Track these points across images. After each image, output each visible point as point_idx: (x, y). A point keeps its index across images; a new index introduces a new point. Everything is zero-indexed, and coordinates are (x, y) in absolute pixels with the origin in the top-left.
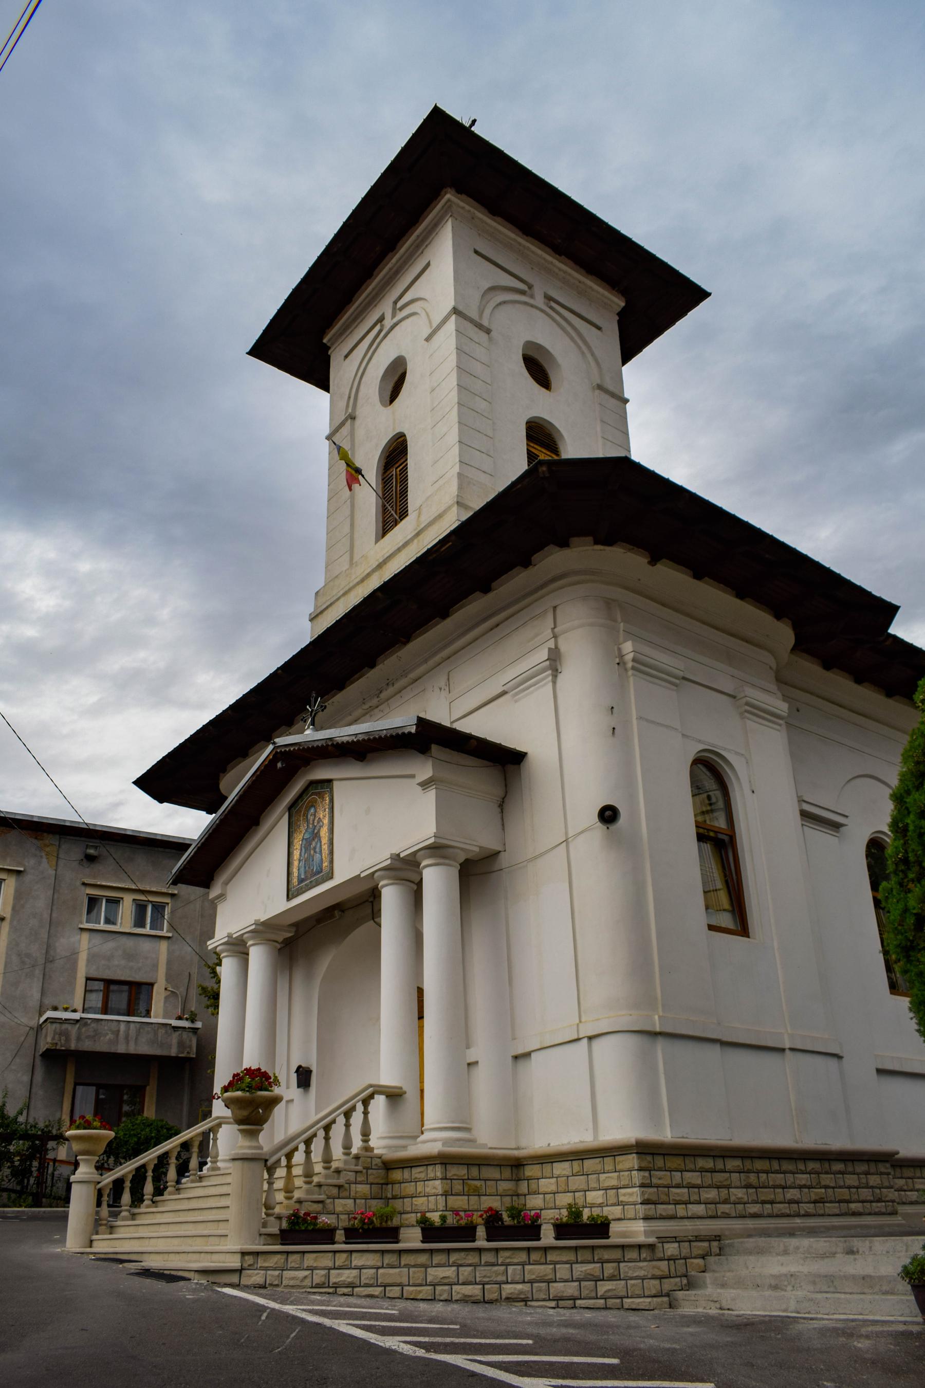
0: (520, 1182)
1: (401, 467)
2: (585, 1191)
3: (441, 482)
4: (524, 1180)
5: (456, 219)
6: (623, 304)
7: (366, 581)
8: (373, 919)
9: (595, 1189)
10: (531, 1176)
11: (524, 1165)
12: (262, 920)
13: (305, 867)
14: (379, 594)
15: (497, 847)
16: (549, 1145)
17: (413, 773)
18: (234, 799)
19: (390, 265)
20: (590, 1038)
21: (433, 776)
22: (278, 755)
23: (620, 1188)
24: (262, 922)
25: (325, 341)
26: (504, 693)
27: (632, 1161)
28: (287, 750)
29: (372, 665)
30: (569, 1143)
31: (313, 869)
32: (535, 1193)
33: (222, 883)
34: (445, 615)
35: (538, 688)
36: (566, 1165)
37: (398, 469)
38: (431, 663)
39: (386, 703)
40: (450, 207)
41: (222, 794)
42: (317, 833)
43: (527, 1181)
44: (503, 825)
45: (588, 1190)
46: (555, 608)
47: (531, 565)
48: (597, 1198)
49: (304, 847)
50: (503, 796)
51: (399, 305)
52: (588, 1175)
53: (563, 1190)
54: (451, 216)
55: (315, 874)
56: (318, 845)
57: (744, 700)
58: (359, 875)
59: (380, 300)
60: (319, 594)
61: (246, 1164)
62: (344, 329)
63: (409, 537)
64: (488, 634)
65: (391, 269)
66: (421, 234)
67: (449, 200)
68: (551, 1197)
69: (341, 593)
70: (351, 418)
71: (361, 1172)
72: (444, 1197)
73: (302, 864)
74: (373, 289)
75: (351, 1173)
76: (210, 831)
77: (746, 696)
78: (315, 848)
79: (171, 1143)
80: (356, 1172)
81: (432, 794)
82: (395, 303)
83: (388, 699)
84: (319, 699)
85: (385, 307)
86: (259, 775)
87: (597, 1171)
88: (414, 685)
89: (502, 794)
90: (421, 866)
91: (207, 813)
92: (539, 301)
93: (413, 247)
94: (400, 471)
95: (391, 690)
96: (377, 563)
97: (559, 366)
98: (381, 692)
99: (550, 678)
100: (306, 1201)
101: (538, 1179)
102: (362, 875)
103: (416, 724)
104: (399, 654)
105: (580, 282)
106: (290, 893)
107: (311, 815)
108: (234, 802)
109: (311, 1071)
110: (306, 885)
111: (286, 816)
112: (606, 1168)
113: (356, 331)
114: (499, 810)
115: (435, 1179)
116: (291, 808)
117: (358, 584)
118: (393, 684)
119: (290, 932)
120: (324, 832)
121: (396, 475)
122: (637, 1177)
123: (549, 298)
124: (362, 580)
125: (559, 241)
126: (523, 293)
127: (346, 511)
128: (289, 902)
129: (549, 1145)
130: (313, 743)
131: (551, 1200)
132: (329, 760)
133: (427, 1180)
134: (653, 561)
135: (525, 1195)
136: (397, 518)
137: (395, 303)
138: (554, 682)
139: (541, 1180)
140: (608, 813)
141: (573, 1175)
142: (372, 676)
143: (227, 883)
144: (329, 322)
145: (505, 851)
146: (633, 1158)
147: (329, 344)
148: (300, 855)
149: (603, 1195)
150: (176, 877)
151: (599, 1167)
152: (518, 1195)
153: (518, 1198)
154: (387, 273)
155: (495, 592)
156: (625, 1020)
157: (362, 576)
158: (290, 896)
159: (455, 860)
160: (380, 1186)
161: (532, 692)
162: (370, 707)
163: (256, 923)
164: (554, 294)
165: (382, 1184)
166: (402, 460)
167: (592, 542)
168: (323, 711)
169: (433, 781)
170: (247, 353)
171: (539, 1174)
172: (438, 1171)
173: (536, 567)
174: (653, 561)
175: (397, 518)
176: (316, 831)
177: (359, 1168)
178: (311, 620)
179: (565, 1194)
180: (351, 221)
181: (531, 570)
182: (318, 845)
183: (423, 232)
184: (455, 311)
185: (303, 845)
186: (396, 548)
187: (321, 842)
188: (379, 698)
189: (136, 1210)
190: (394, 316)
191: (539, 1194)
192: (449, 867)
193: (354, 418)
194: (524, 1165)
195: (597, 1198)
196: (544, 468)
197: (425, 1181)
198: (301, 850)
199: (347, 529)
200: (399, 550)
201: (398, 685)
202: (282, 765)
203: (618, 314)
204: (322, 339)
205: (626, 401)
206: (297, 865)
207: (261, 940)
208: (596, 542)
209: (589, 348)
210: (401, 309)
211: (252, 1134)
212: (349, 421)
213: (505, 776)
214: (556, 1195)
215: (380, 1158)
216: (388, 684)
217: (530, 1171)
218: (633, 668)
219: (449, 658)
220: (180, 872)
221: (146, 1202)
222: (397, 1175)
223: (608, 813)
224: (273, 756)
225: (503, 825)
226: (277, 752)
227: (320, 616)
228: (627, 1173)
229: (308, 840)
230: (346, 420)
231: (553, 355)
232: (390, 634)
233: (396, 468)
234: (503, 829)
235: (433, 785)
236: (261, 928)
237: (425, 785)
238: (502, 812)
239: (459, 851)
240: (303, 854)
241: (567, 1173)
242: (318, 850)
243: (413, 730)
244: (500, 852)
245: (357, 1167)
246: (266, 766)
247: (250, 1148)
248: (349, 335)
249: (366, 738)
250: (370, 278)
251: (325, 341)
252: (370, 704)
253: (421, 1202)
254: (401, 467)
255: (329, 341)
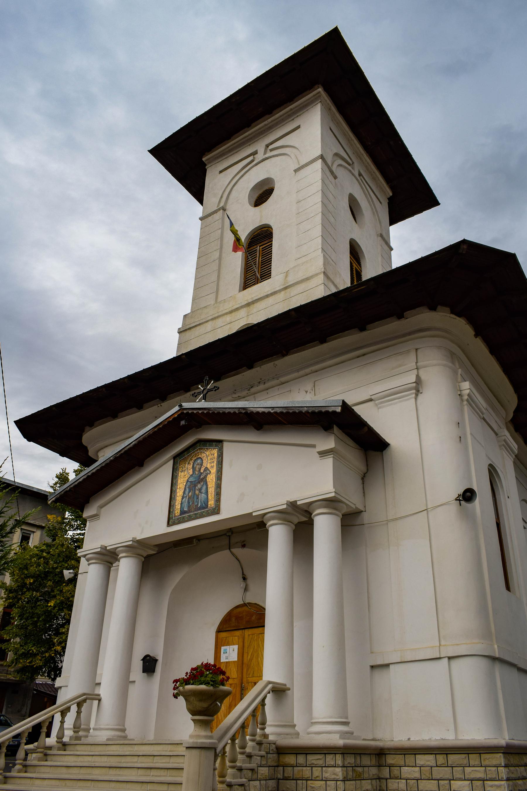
0: (382, 768)
1: (264, 246)
2: (450, 780)
3: (304, 259)
4: (386, 766)
5: (323, 105)
6: (391, 194)
7: (234, 313)
8: (230, 549)
9: (460, 779)
10: (394, 764)
11: (385, 754)
12: (137, 539)
13: (189, 502)
14: (293, 313)
15: (362, 508)
16: (409, 739)
17: (313, 443)
18: (132, 443)
19: (266, 122)
20: (450, 658)
21: (335, 447)
22: (183, 414)
23: (487, 780)
24: (137, 540)
25: (204, 159)
26: (371, 400)
27: (499, 759)
28: (190, 412)
29: (251, 367)
30: (430, 739)
31: (198, 504)
32: (397, 778)
33: (98, 506)
34: (323, 341)
35: (400, 402)
36: (431, 757)
37: (261, 247)
38: (302, 373)
39: (253, 396)
40: (320, 96)
41: (83, 444)
42: (203, 478)
43: (388, 768)
44: (364, 492)
45: (453, 780)
46: (417, 349)
47: (404, 318)
48: (464, 787)
49: (189, 488)
50: (365, 472)
51: (271, 147)
52: (452, 767)
53: (427, 778)
54: (320, 102)
55: (200, 509)
56: (204, 487)
57: (503, 438)
58: (252, 513)
59: (254, 142)
60: (187, 317)
61: (203, 752)
62: (221, 155)
63: (278, 289)
64: (354, 360)
65: (266, 125)
66: (294, 108)
67: (319, 92)
68: (414, 783)
69: (210, 318)
70: (223, 210)
71: (264, 756)
72: (343, 782)
73: (186, 500)
74: (249, 135)
75: (258, 757)
76: (103, 465)
77: (505, 435)
78: (200, 490)
79: (45, 714)
80: (261, 756)
81: (329, 461)
82: (267, 146)
83: (254, 394)
84: (212, 382)
85: (260, 146)
86: (160, 428)
87: (462, 764)
88: (281, 386)
89: (365, 470)
90: (313, 514)
91: (60, 455)
92: (357, 174)
93: (286, 115)
94: (262, 248)
95: (262, 387)
96: (246, 302)
97: (363, 215)
98: (252, 387)
99: (414, 395)
100: (235, 785)
101: (400, 767)
102: (254, 514)
103: (341, 406)
104: (276, 362)
105: (374, 172)
106: (171, 521)
107: (198, 464)
108: (131, 445)
109: (156, 660)
110: (189, 516)
111: (171, 462)
112: (472, 763)
113: (231, 158)
114: (361, 481)
115: (335, 767)
116: (176, 458)
117: (226, 314)
118: (264, 383)
119: (154, 550)
120: (211, 479)
121: (259, 250)
122: (503, 772)
123: (360, 175)
124: (231, 312)
125: (369, 143)
126: (349, 164)
127: (214, 267)
128: (169, 527)
129: (409, 739)
130: (224, 410)
131: (414, 785)
132: (229, 426)
133: (325, 767)
134: (476, 336)
135: (386, 779)
136: (259, 277)
137: (267, 146)
138: (416, 399)
139: (404, 768)
140: (468, 494)
141: (437, 766)
142: (248, 375)
143: (101, 507)
144: (210, 149)
145: (365, 511)
146: (500, 756)
147: (206, 162)
148: (184, 493)
149: (469, 784)
150: (60, 496)
151: (465, 762)
152: (379, 779)
153: (380, 781)
154: (263, 127)
155: (369, 331)
156: (479, 647)
157: (230, 309)
158: (170, 523)
159: (340, 511)
160: (274, 768)
161: (396, 403)
162: (239, 396)
163: (134, 541)
164: (363, 173)
165: (275, 766)
166: (255, 247)
167: (450, 312)
168: (215, 390)
169: (332, 451)
170: (148, 151)
171: (402, 763)
172: (339, 760)
173: (407, 320)
174: (476, 336)
175: (259, 277)
176: (202, 477)
177: (263, 753)
178: (180, 332)
179: (429, 781)
180: (253, 84)
181: (403, 322)
182: (204, 487)
183: (296, 107)
184: (322, 157)
185: (187, 486)
186: (265, 294)
187: (207, 486)
188: (249, 391)
189: (8, 774)
190: (265, 153)
191: (401, 779)
192: (337, 517)
193: (225, 210)
194: (385, 754)
195: (464, 787)
196: (465, 247)
197: (322, 767)
198: (185, 489)
199: (214, 278)
200: (267, 296)
201: (268, 385)
202: (185, 423)
203: (389, 199)
204: (202, 158)
205: (392, 249)
206: (180, 500)
207: (133, 554)
208: (452, 312)
209: (376, 211)
210: (271, 150)
211: (206, 724)
212: (221, 211)
213: (366, 458)
214: (419, 781)
215: (275, 744)
216: (259, 383)
217: (390, 760)
218: (467, 400)
219: (317, 371)
220: (65, 492)
221: (17, 767)
222: (290, 759)
223: (468, 494)
224: (178, 415)
225: (364, 492)
226: (183, 413)
227: (188, 331)
228: (494, 769)
229: (194, 483)
230: (219, 209)
231: (361, 207)
232: (278, 346)
233: (260, 246)
234: (364, 496)
235: (332, 454)
236: (136, 544)
237: (323, 454)
238: (363, 484)
239: (345, 506)
240: (187, 492)
241: (431, 764)
242: (203, 490)
243: (339, 410)
244: (362, 511)
245: (260, 752)
246: (169, 422)
247: (206, 737)
248: (224, 159)
249: (284, 411)
250: (248, 127)
251: (204, 159)
252: (239, 395)
253: (319, 785)
254: (264, 246)
255: (206, 160)
